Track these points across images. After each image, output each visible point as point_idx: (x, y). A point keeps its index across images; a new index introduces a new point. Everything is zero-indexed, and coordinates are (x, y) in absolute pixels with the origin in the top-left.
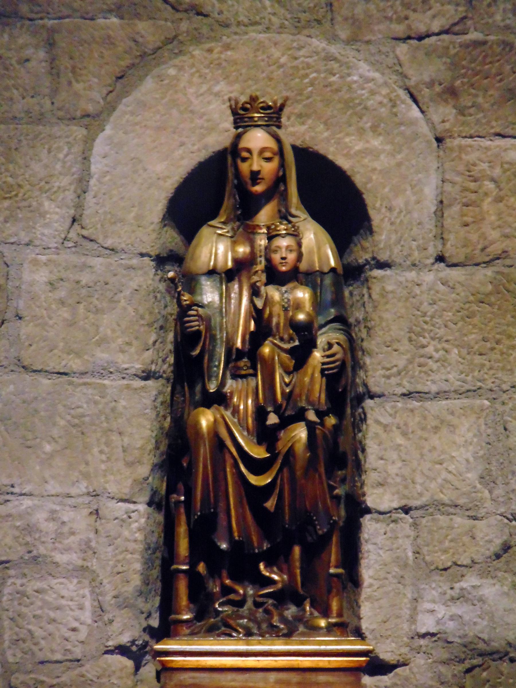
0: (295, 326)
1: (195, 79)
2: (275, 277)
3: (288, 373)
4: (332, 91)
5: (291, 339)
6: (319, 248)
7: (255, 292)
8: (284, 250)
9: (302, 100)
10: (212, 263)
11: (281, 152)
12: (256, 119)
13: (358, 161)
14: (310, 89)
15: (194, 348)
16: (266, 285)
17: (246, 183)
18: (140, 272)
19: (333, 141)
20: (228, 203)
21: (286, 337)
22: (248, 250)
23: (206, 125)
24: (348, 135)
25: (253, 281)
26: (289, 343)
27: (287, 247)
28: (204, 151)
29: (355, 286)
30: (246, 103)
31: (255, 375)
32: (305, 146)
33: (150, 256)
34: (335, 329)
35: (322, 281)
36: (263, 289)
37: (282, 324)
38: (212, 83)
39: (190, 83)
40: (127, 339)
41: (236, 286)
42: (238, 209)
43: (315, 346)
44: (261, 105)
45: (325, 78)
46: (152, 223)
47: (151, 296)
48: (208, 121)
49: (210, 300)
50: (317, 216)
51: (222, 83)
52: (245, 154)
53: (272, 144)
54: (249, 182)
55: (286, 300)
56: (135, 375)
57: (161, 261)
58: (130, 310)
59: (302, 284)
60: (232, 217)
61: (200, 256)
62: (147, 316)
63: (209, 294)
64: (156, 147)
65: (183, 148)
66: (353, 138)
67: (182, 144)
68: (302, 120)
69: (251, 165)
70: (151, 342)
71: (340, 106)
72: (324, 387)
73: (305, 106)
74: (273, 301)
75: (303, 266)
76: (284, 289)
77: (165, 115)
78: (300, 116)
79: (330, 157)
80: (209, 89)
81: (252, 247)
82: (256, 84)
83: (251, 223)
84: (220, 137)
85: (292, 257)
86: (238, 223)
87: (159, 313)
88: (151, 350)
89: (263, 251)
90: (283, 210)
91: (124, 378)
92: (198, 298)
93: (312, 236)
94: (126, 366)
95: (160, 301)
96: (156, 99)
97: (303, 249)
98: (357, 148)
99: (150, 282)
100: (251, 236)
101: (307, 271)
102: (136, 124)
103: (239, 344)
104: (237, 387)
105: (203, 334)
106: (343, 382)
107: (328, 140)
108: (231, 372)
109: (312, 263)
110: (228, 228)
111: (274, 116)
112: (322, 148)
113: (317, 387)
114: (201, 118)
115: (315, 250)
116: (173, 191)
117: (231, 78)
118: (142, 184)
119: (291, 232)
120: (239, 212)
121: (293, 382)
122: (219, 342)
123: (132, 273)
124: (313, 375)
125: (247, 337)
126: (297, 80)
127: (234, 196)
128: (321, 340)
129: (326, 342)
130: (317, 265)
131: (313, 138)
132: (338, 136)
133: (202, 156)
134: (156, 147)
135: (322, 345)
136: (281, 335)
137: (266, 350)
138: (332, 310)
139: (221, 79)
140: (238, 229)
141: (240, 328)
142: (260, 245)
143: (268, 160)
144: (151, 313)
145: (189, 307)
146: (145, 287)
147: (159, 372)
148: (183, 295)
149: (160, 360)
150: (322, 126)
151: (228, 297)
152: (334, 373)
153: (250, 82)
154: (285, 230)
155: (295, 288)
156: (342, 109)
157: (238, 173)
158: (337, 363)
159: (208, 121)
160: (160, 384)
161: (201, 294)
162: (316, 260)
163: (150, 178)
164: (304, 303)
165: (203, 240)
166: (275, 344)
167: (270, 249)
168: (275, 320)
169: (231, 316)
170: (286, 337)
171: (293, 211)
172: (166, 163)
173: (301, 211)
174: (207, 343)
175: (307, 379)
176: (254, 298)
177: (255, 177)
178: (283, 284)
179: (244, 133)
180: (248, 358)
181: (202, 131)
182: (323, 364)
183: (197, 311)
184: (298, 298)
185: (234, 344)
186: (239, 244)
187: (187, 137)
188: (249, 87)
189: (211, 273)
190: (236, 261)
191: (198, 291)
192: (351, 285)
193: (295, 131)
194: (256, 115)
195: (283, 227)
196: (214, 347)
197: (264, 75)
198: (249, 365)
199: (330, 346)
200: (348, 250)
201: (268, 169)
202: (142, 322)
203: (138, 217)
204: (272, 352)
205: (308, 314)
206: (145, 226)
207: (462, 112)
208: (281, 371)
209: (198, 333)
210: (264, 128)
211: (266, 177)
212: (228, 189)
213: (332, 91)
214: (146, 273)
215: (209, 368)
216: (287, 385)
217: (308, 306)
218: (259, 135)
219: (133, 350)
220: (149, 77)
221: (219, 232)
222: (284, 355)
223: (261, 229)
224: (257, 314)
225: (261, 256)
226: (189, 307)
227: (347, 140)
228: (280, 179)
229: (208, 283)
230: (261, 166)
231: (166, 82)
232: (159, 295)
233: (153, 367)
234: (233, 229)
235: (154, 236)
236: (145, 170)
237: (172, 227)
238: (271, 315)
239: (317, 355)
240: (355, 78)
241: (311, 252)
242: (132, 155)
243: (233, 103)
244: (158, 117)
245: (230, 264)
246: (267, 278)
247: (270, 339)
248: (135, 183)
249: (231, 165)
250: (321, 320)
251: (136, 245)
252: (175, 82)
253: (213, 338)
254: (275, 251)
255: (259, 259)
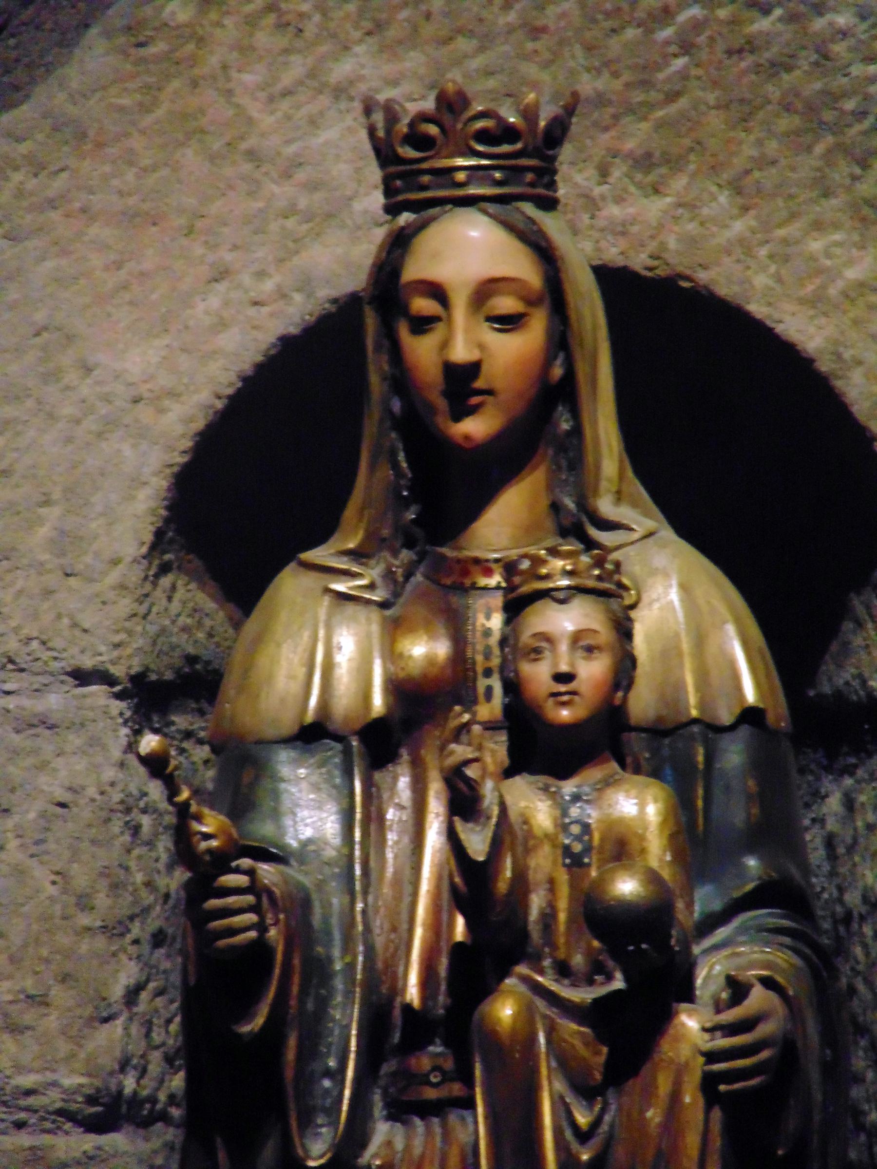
0: (603, 920)
1: (263, 39)
2: (542, 747)
3: (587, 1092)
4: (757, 68)
5: (597, 970)
6: (700, 641)
7: (464, 803)
8: (564, 647)
9: (652, 106)
10: (313, 701)
11: (555, 295)
12: (461, 176)
13: (856, 322)
14: (680, 62)
15: (246, 1012)
16: (509, 773)
17: (432, 409)
18: (75, 740)
19: (763, 252)
20: (369, 483)
21: (578, 960)
22: (442, 649)
23: (303, 203)
24: (818, 226)
25: (450, 761)
26: (591, 982)
27: (576, 638)
28: (298, 297)
29: (860, 773)
30: (424, 117)
31: (469, 1104)
32: (661, 272)
33: (108, 680)
34: (761, 929)
35: (710, 759)
36: (488, 788)
37: (562, 917)
38: (324, 48)
39: (245, 49)
40: (29, 984)
41: (404, 782)
42: (406, 503)
43: (688, 995)
44: (480, 124)
45: (734, 22)
46: (115, 562)
47: (116, 826)
48: (313, 186)
49: (307, 833)
50: (697, 523)
51: (359, 49)
52: (422, 305)
53: (521, 266)
54: (442, 404)
55: (575, 829)
56: (60, 1112)
57: (151, 697)
58: (41, 875)
59: (637, 771)
60: (386, 532)
61: (270, 679)
62: (102, 900)
63: (308, 813)
64: (125, 287)
65: (221, 287)
66: (837, 237)
67: (221, 274)
68: (651, 178)
69: (445, 345)
70: (117, 992)
71: (785, 123)
72: (717, 1142)
73: (660, 125)
74: (529, 834)
75: (642, 703)
76: (569, 787)
77: (154, 168)
78: (644, 162)
79: (756, 309)
80: (312, 74)
81: (459, 641)
82: (482, 49)
83: (446, 551)
84: (341, 261)
85: (592, 671)
86: (406, 555)
87: (148, 884)
88: (119, 1022)
89: (496, 651)
90: (569, 503)
91: (20, 1125)
92: (263, 830)
93: (674, 595)
94: (27, 1081)
95: (150, 844)
96: (121, 109)
97: (640, 644)
98: (852, 274)
99: (110, 773)
100: (455, 600)
101: (660, 719)
102: (51, 204)
103: (413, 993)
104: (408, 1148)
105: (279, 957)
106: (792, 1123)
107: (745, 246)
108: (385, 1094)
109: (672, 693)
110: (373, 572)
111: (525, 165)
112: (723, 278)
113: (692, 1141)
114: (287, 175)
115: (686, 646)
116: (188, 444)
117: (392, 33)
118: (78, 422)
119: (591, 583)
120: (411, 516)
121: (604, 1128)
122: (339, 984)
123: (46, 743)
124: (675, 1097)
125: (443, 965)
126: (631, 33)
127: (393, 454)
128: (710, 973)
129: (722, 980)
130: (692, 699)
131: (692, 242)
132: (781, 232)
133: (293, 314)
134: (125, 287)
135: (713, 988)
136: (561, 954)
137: (505, 1011)
138: (752, 862)
139: (357, 34)
140: (408, 576)
141: (419, 930)
142: (487, 633)
143: (508, 323)
144: (115, 887)
145: (222, 861)
146: (92, 792)
147: (152, 1100)
148: (199, 818)
149: (156, 1057)
150: (723, 198)
151: (374, 819)
152: (754, 1090)
153: (463, 44)
154: (570, 574)
155: (608, 783)
156: (798, 133)
157: (402, 379)
158: (765, 1054)
159: (313, 186)
160: (156, 1143)
161: (276, 814)
162: (690, 680)
163: (107, 399)
164: (642, 838)
165: (283, 616)
166: (539, 990)
167: (515, 648)
168: (537, 902)
169: (386, 890)
170: (578, 960)
171: (606, 507)
172: (166, 340)
173: (635, 504)
174: (295, 989)
175: (654, 1115)
176: (456, 819)
177: (463, 384)
178: (564, 774)
179: (421, 227)
180: (446, 1044)
181: (290, 223)
182: (711, 1057)
183: (251, 873)
184: (621, 821)
185: (397, 989)
186: (412, 630)
187: (235, 247)
188: (458, 61)
189: (312, 735)
190: (396, 688)
191: (267, 804)
192: (849, 771)
193: (614, 216)
194: (461, 162)
195: (559, 563)
196: (323, 1003)
197: (512, 17)
198: (449, 1065)
199: (737, 989)
200: (834, 647)
201: (511, 355)
202: (85, 920)
203: (65, 541)
204: (527, 1014)
205: (652, 878)
206: (97, 573)
207: (671, 169)
208: (560, 1086)
209: (260, 951)
210: (492, 208)
211: (499, 384)
212: (370, 428)
213: (757, 68)
214: (95, 742)
215: (306, 1079)
216: (584, 1136)
217: (657, 851)
218: (474, 234)
219: (52, 1022)
220: (94, 31)
221: (340, 587)
222: (570, 1027)
223: (488, 572)
224: (469, 883)
225: (488, 673)
226: (222, 861)
227: (816, 245)
228: (554, 392)
229: (302, 772)
230: (481, 347)
231: (158, 47)
232: (146, 821)
233: (129, 1084)
234: (389, 575)
235: (125, 605)
236: (88, 370)
237: (193, 575)
238: (521, 884)
239: (690, 1022)
240: (842, 20)
241: (669, 654)
242: (40, 317)
243: (378, 118)
244: (130, 175)
245: (378, 702)
246: (513, 750)
247: (522, 969)
248: (51, 416)
249: (378, 348)
250: (706, 899)
251: (57, 643)
252: (191, 47)
253: (317, 972)
254: (535, 654)
255: (482, 684)
